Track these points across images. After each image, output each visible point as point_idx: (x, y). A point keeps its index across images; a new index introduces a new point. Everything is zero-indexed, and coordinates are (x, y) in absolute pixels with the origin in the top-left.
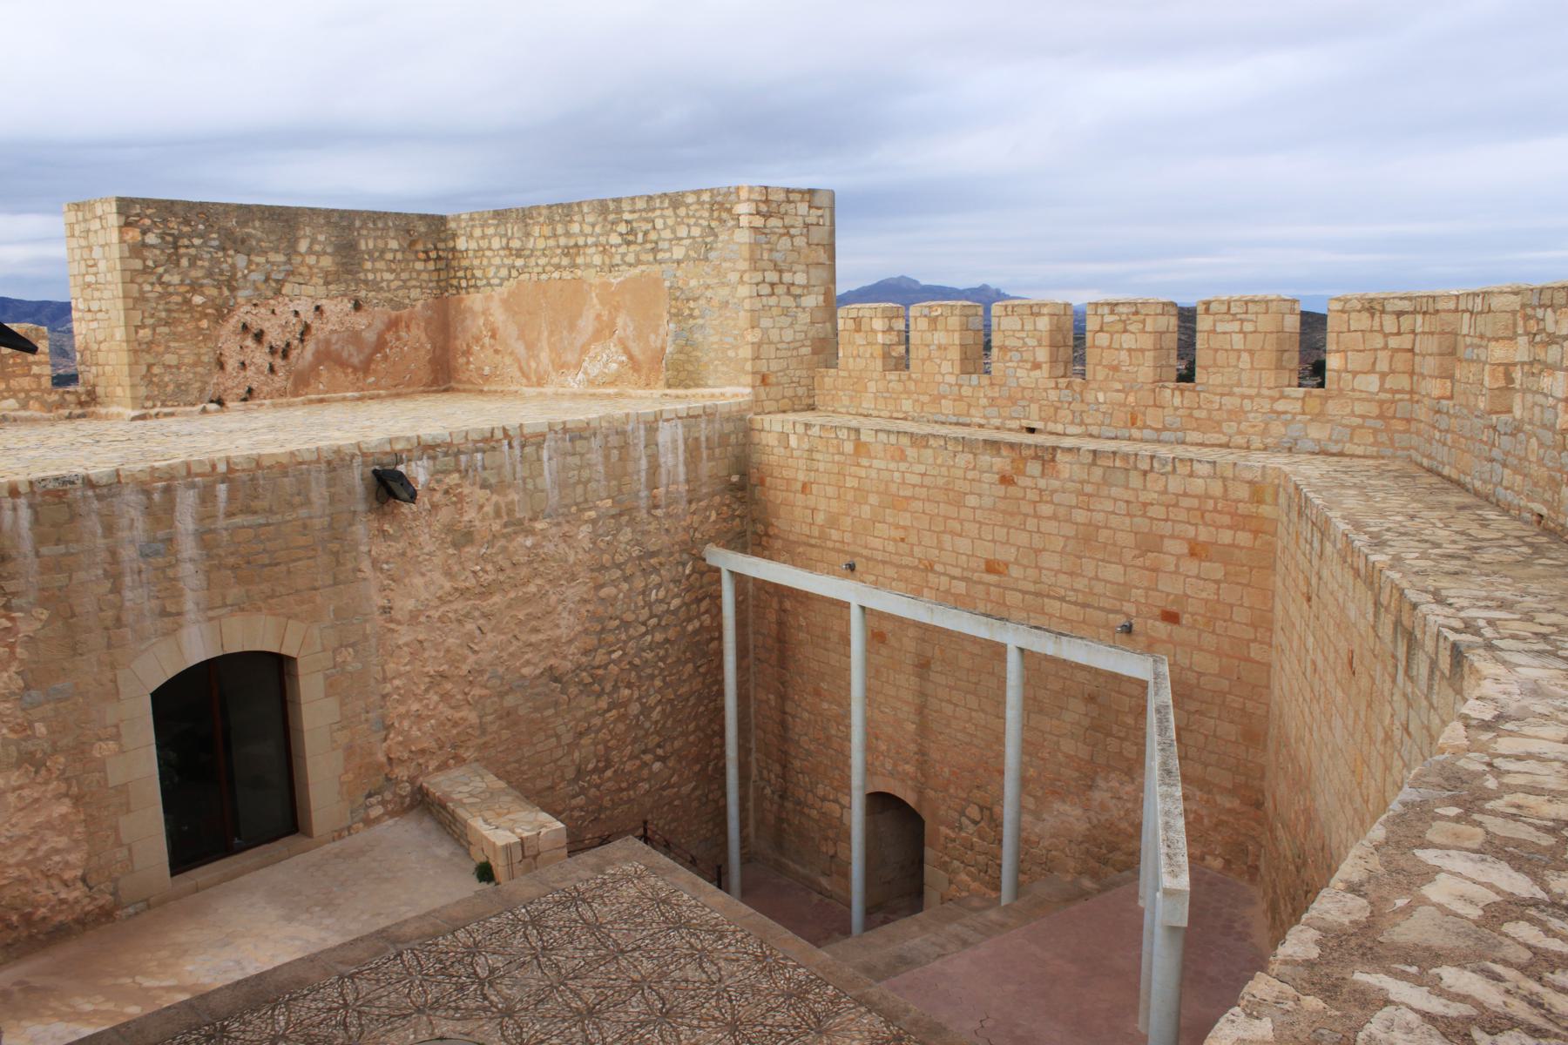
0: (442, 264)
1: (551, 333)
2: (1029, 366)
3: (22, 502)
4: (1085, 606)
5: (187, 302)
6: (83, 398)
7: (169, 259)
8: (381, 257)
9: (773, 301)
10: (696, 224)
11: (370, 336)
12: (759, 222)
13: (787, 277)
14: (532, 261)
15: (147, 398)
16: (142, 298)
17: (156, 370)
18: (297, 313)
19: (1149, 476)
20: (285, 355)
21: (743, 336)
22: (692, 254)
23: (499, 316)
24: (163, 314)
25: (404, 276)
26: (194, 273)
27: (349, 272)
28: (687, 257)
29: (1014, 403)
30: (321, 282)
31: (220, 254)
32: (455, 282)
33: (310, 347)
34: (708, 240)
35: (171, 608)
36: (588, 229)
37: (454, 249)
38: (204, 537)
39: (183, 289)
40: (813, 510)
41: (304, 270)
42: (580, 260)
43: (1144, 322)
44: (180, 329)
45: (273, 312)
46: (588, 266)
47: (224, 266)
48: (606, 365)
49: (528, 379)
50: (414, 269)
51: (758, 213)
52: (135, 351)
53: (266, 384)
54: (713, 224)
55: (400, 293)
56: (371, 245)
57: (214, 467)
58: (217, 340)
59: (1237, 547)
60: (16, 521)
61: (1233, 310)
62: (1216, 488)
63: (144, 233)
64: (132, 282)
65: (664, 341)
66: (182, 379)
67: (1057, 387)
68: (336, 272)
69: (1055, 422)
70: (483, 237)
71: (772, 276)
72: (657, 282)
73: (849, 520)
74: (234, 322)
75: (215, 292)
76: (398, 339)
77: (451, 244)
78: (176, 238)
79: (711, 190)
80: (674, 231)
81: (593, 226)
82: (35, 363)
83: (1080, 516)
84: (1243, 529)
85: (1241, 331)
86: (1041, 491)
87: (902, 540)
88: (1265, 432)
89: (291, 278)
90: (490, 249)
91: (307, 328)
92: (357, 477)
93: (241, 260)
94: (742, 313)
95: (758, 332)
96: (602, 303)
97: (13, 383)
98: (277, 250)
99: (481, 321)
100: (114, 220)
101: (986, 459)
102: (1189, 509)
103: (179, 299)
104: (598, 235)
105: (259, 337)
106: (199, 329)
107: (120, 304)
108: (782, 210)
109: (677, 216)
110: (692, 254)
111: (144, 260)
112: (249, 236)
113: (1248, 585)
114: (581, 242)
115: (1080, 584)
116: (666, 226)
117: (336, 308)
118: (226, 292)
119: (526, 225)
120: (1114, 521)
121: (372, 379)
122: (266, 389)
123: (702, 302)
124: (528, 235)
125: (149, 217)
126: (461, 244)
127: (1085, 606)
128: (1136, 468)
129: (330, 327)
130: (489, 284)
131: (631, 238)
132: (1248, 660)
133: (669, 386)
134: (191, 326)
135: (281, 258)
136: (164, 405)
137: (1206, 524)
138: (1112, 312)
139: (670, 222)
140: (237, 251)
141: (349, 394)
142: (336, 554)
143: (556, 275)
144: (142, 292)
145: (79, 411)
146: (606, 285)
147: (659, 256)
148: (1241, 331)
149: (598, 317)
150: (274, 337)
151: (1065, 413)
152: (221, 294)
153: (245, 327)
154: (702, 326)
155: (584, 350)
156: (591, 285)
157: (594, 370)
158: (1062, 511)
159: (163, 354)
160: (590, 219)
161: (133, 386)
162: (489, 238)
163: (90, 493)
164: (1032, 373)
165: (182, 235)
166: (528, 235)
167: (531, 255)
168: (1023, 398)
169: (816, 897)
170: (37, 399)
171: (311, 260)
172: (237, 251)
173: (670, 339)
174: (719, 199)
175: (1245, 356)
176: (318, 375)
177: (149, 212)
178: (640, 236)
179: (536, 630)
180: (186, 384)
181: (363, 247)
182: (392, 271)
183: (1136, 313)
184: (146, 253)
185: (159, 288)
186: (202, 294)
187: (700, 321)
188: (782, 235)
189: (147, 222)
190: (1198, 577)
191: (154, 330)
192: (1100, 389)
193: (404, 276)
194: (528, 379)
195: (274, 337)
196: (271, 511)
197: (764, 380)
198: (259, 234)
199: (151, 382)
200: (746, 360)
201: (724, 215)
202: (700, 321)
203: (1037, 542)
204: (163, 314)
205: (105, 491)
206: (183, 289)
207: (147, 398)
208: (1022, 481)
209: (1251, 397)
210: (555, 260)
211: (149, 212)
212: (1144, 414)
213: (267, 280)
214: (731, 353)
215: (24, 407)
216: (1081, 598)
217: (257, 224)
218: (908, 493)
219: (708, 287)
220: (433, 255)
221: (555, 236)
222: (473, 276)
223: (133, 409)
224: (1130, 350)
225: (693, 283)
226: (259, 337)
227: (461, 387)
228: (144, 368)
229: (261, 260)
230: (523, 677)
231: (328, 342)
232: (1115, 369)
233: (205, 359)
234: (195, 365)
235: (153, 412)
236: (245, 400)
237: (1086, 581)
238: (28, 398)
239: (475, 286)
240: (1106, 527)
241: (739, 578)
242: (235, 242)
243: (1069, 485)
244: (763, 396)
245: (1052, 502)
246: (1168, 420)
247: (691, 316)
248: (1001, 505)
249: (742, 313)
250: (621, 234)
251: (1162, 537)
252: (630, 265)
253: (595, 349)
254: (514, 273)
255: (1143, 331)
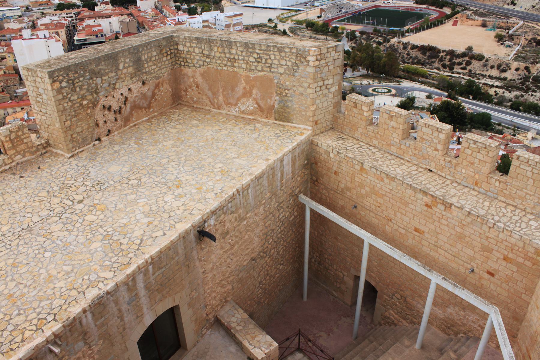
0: (173, 55)
1: (224, 91)
2: (433, 149)
3: (88, 313)
4: (454, 256)
5: (81, 105)
6: (45, 145)
7: (72, 90)
8: (150, 60)
9: (321, 93)
10: (289, 61)
11: (149, 94)
12: (317, 63)
13: (326, 82)
14: (214, 61)
15: (73, 148)
16: (65, 110)
17: (74, 136)
18: (122, 94)
19: (491, 229)
20: (120, 112)
21: (309, 108)
22: (287, 72)
23: (199, 79)
24: (73, 113)
25: (159, 65)
26: (82, 92)
27: (139, 71)
28: (285, 73)
29: (425, 159)
30: (129, 78)
31: (91, 81)
32: (179, 62)
33: (129, 106)
34: (295, 68)
35: (139, 314)
36: (239, 53)
37: (177, 49)
38: (147, 288)
39: (79, 100)
40: (339, 182)
41: (123, 76)
42: (236, 64)
43: (488, 152)
44: (81, 116)
45: (113, 97)
46: (240, 67)
47: (93, 85)
48: (248, 107)
49: (214, 106)
50: (163, 61)
51: (317, 60)
52: (66, 132)
53: (114, 126)
54: (297, 62)
55: (159, 72)
56: (146, 57)
57: (147, 262)
58: (94, 116)
59: (525, 265)
60: (87, 320)
61: (530, 163)
62: (521, 244)
63: (61, 83)
64: (60, 105)
65: (274, 103)
66: (84, 136)
67: (444, 160)
68: (135, 73)
69: (442, 172)
70: (191, 47)
71: (321, 83)
72: (271, 80)
73: (355, 192)
74: (100, 106)
75: (91, 97)
76: (160, 91)
77: (176, 47)
78: (73, 80)
79: (297, 48)
80: (279, 61)
81: (242, 52)
82: (25, 138)
83: (459, 230)
84: (529, 261)
85: (531, 171)
86: (443, 215)
87: (379, 207)
88: (533, 208)
89: (118, 81)
90: (194, 52)
91: (126, 98)
92: (192, 237)
93: (99, 80)
94: (309, 99)
95: (315, 106)
96: (247, 83)
97: (18, 149)
98: (111, 72)
99: (192, 80)
100: (48, 80)
101: (420, 196)
102: (506, 246)
103: (78, 105)
104: (244, 56)
105: (109, 109)
106: (87, 114)
107: (56, 114)
108: (326, 56)
109: (281, 56)
110: (287, 72)
111: (63, 94)
112: (101, 69)
113: (527, 277)
114: (236, 57)
115: (454, 249)
116: (275, 59)
117: (136, 87)
118: (95, 95)
119: (211, 46)
120: (473, 237)
121: (152, 110)
122: (114, 128)
123: (291, 91)
124: (212, 50)
125: (61, 75)
126: (181, 48)
127: (454, 256)
128: (486, 225)
129: (135, 95)
130: (194, 66)
131: (259, 60)
132: (520, 298)
133: (276, 120)
134: (84, 114)
135: (114, 74)
136: (79, 148)
137: (512, 253)
138: (474, 144)
139: (278, 57)
140: (97, 78)
141: (144, 119)
142: (188, 265)
143: (225, 68)
144: (64, 107)
145: (44, 151)
146: (248, 77)
147: (272, 70)
148: (531, 171)
149: (245, 88)
150: (115, 107)
151: (446, 170)
152: (93, 97)
153: (104, 107)
154: (291, 101)
155: (239, 99)
156: (241, 75)
157: (243, 108)
158: (451, 225)
159: (75, 129)
160: (241, 49)
161: (67, 145)
162: (194, 48)
163: (109, 296)
164: (434, 152)
165: (75, 78)
166: (212, 50)
167: (213, 58)
168: (429, 159)
169: (332, 298)
170: (28, 152)
171: (125, 71)
172: (97, 78)
173: (276, 103)
174: (300, 52)
175: (531, 180)
176: (133, 115)
177: (61, 73)
178: (264, 61)
179: (247, 249)
180: (86, 137)
181: (143, 59)
182: (155, 65)
183: (485, 148)
184: (63, 91)
185: (70, 103)
186: (86, 99)
187: (290, 99)
188: (325, 66)
189: (61, 78)
190: (505, 267)
191: (71, 120)
192: (464, 168)
193: (159, 65)
194: (214, 106)
195: (115, 107)
196: (167, 264)
197: (316, 123)
198: (104, 67)
199: (73, 141)
200: (310, 117)
201: (302, 60)
202: (290, 99)
203: (438, 230)
204: (73, 113)
205: (114, 292)
206: (79, 100)
207: (73, 148)
208: (435, 209)
209: (530, 195)
210: (225, 62)
211: (61, 73)
212: (481, 183)
213: (110, 84)
214: (303, 113)
215: (24, 156)
216: (454, 254)
217: (103, 63)
218: (384, 193)
219: (294, 86)
220: (169, 53)
221: (224, 53)
222: (187, 62)
223: (68, 154)
224: (480, 160)
225: (287, 83)
226: (109, 109)
227: (184, 103)
228: (70, 137)
229: (106, 77)
230: (244, 266)
231: (134, 101)
232: (472, 164)
233: (91, 125)
234: (88, 129)
235: (76, 152)
236: (108, 135)
237: (457, 250)
238: (25, 152)
239: (188, 66)
240: (469, 237)
241: (312, 211)
242: (95, 74)
243: (456, 218)
244: (316, 129)
245: (447, 220)
246: (491, 189)
247: (286, 96)
248: (425, 213)
249: (309, 99)
250: (255, 58)
251: (493, 250)
252: (259, 71)
253: (243, 100)
254: (206, 64)
255: (487, 155)
